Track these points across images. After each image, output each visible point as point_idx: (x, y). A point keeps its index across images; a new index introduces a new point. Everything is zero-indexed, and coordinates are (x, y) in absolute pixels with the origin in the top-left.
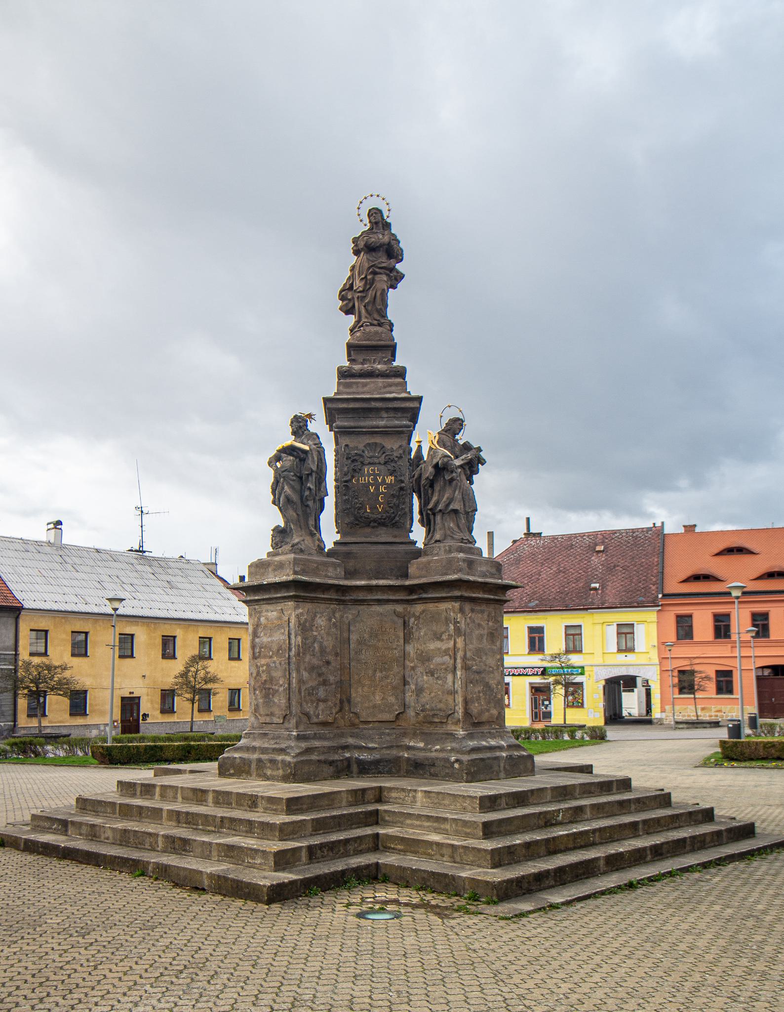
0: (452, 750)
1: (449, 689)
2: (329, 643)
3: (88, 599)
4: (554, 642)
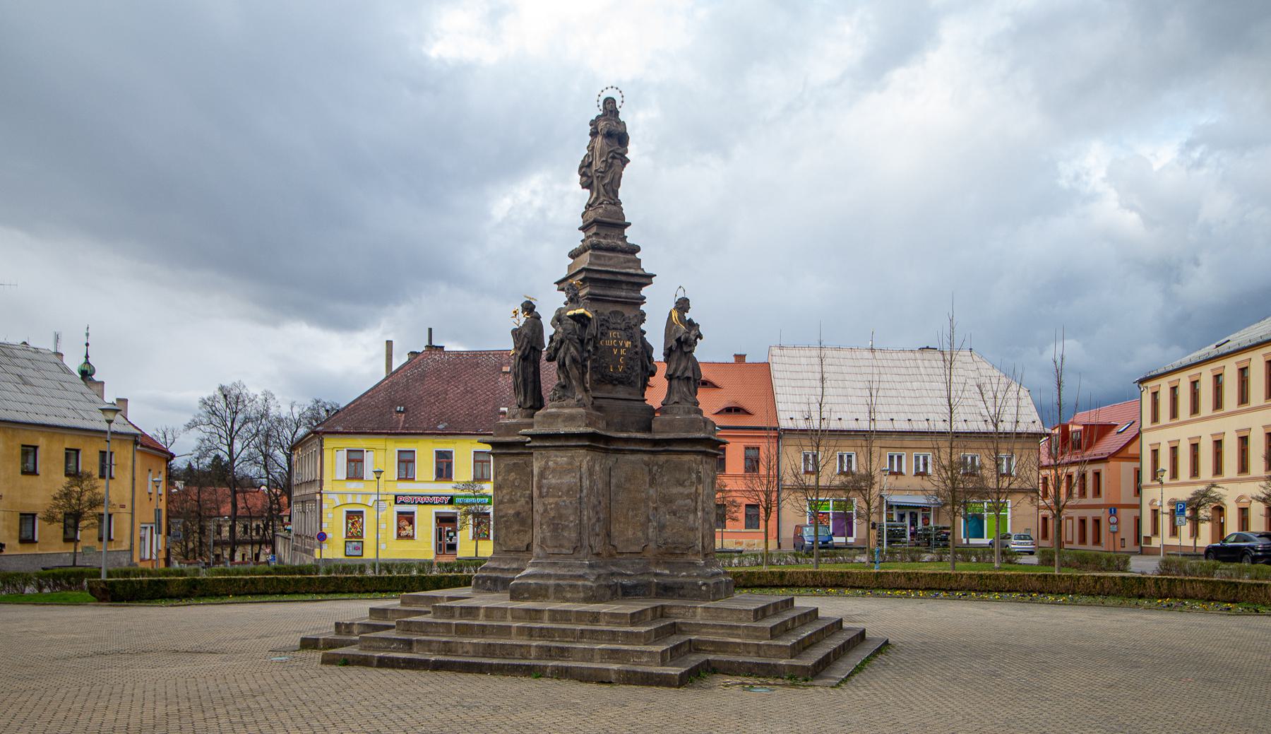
0: (698, 575)
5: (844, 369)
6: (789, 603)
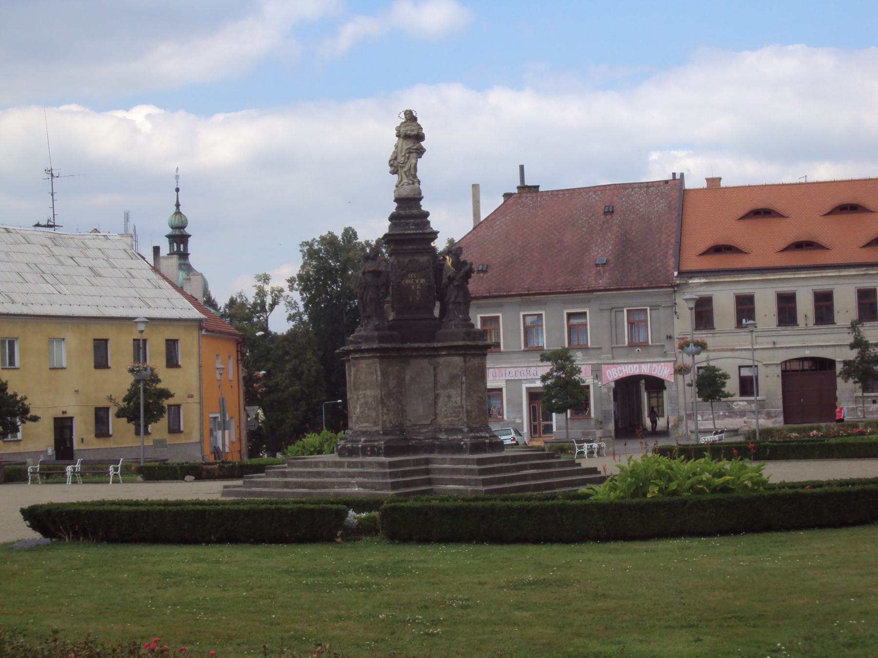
1: (453, 402)
3: (16, 297)
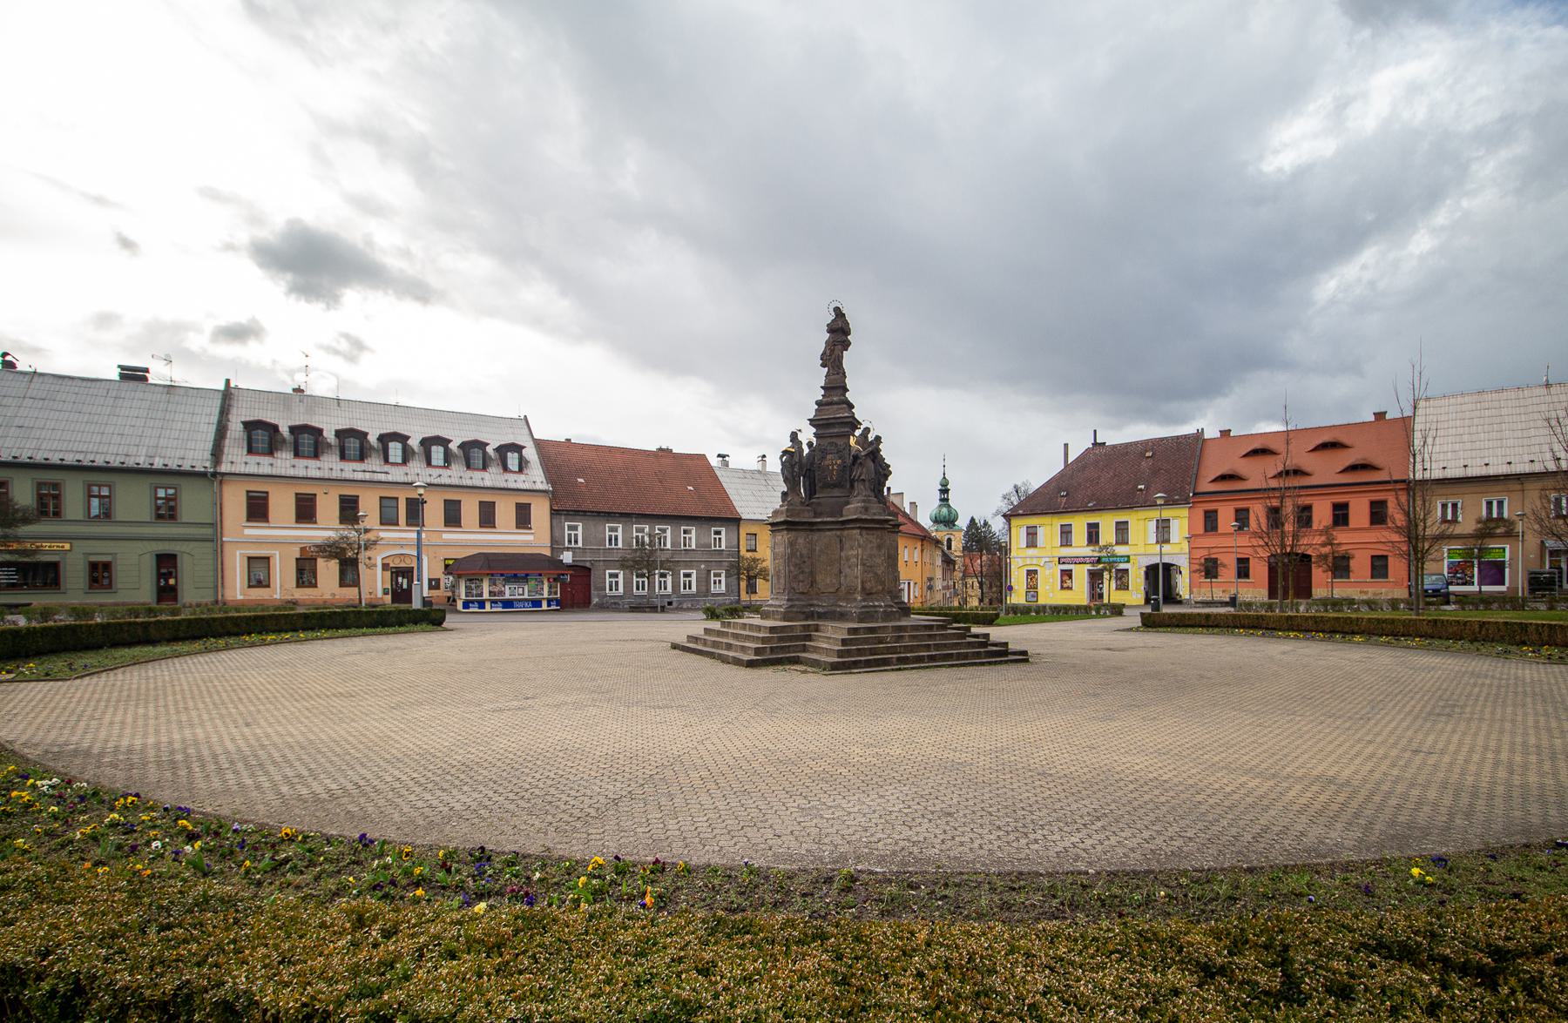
2: (805, 552)
4: (1107, 535)
5: (1504, 411)
6: (968, 629)
